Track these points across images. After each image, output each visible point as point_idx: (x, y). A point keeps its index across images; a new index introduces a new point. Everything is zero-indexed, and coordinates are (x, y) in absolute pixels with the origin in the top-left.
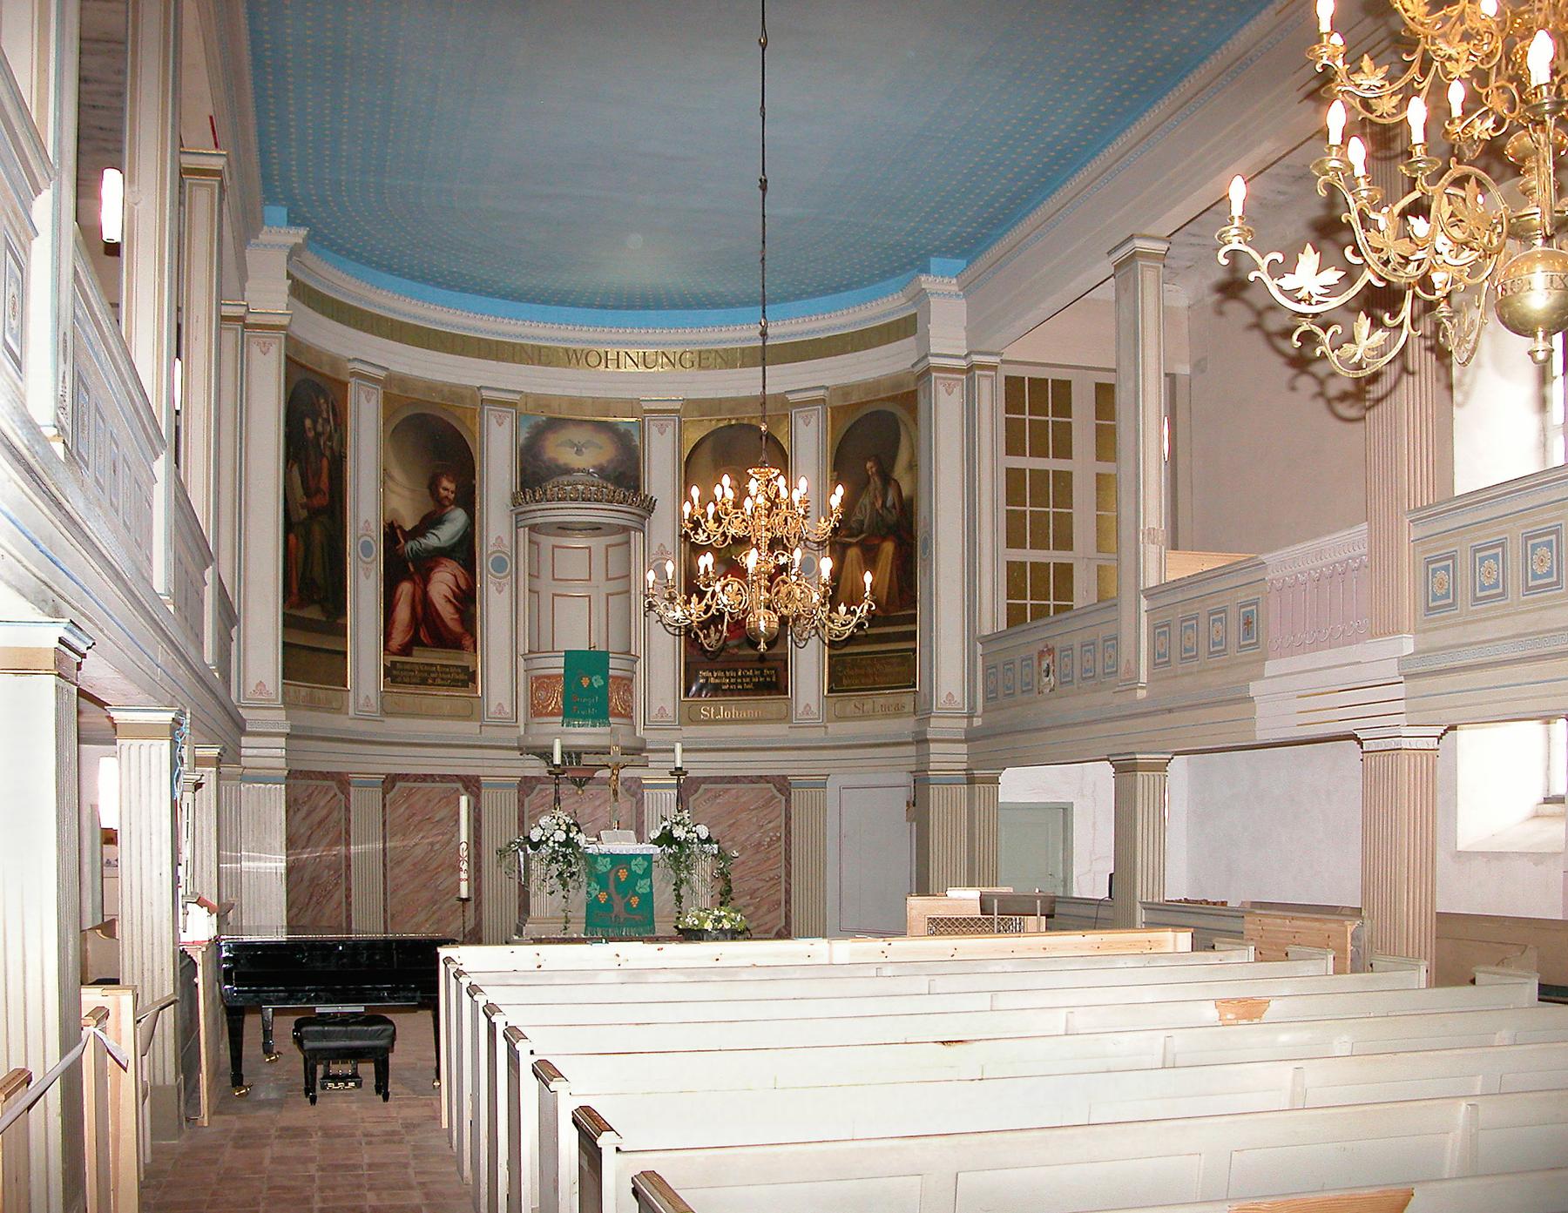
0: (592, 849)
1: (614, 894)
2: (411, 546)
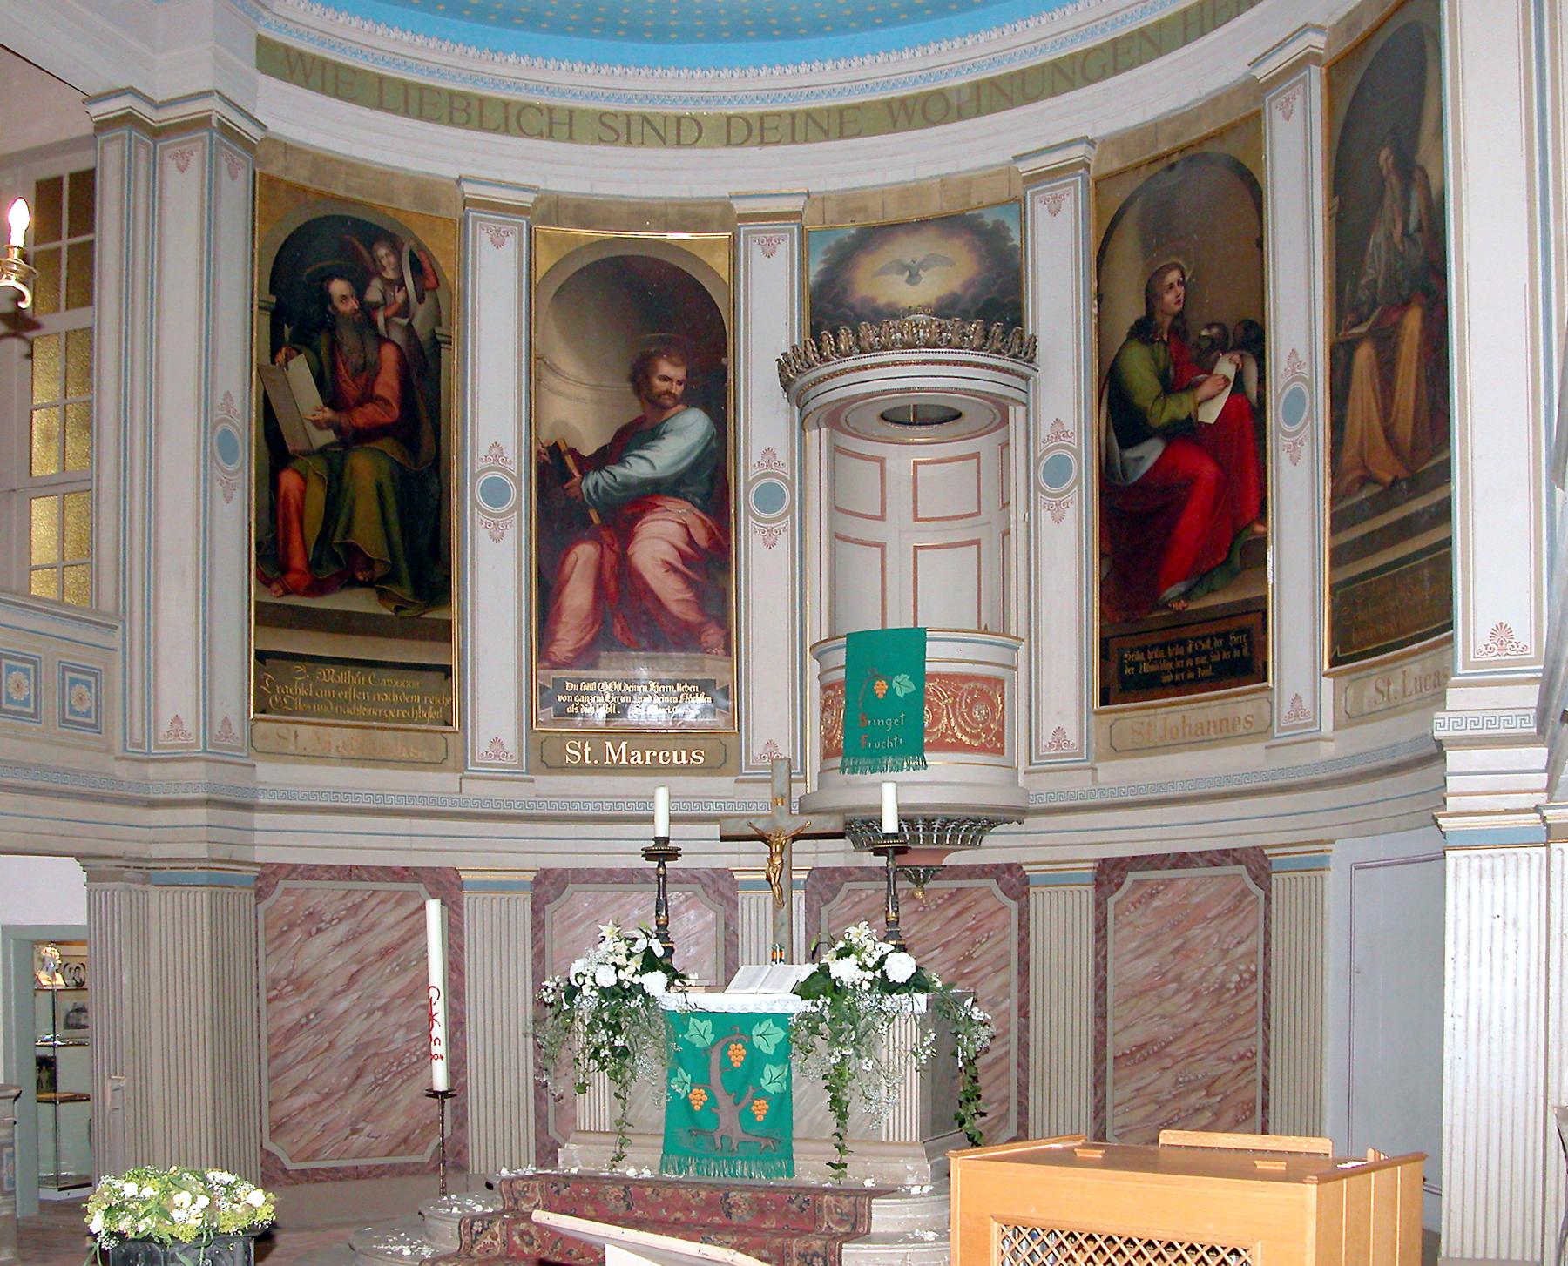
0: (672, 1002)
1: (720, 1094)
2: (593, 481)
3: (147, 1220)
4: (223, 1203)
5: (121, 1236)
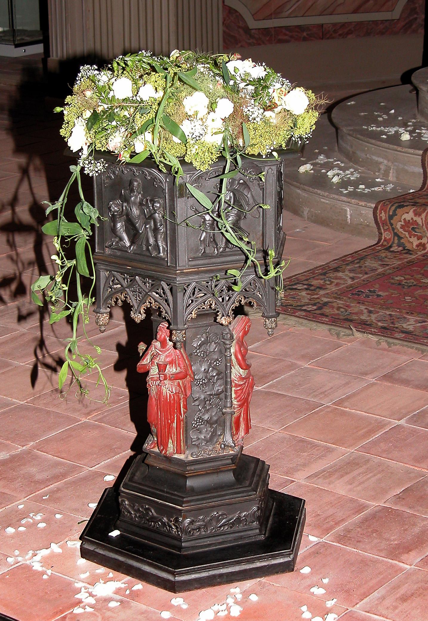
3: (148, 136)
4: (255, 111)
5: (110, 156)
